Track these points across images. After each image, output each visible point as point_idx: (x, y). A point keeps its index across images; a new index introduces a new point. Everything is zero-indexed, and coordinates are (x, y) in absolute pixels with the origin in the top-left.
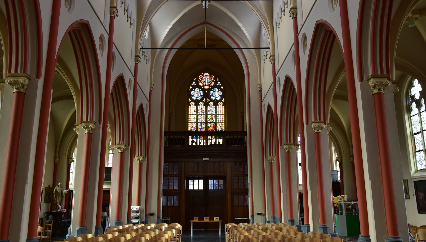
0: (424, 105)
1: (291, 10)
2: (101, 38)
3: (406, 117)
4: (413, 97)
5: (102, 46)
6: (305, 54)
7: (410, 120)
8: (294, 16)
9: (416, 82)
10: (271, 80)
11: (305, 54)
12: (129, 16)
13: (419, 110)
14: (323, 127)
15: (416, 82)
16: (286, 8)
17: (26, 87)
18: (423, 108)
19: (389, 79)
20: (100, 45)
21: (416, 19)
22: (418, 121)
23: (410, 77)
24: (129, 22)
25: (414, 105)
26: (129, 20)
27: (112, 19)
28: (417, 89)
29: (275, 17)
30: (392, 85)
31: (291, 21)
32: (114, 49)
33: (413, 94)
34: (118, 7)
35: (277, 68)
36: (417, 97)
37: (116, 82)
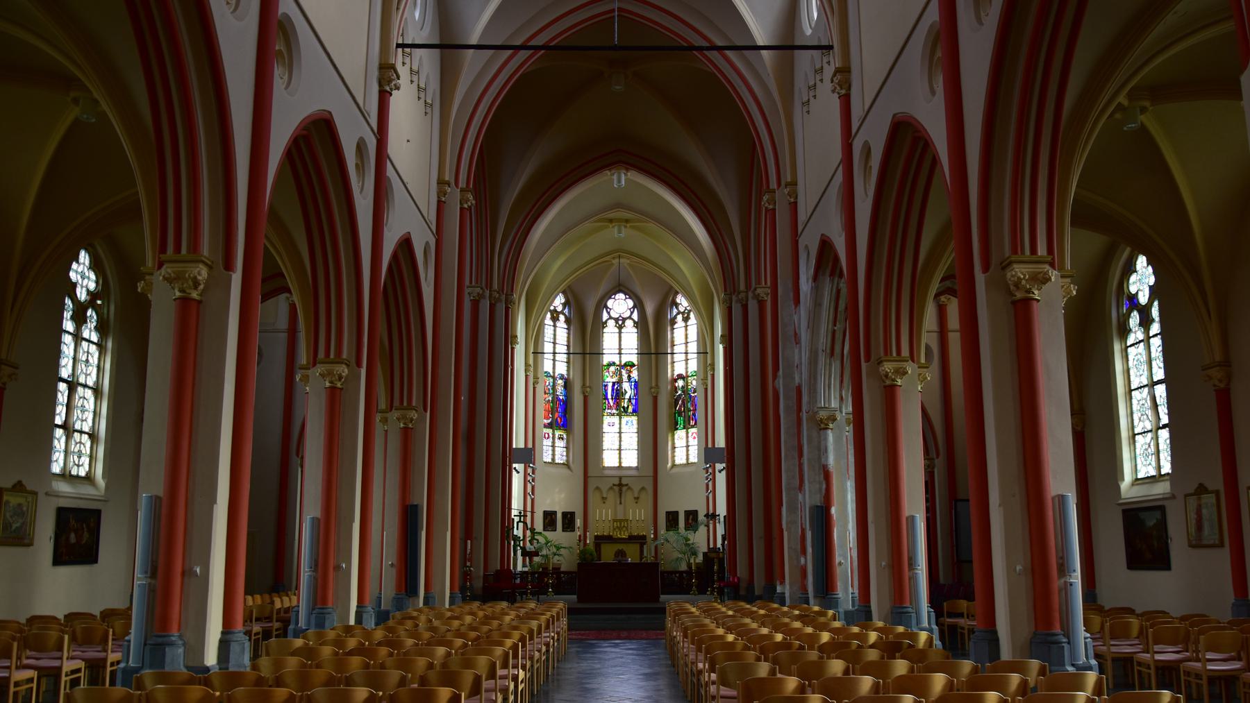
0: (1157, 319)
1: (834, 75)
2: (361, 147)
3: (1117, 347)
4: (1133, 299)
5: (361, 167)
6: (980, 22)
7: (1126, 357)
8: (843, 92)
9: (1142, 261)
10: (837, 154)
11: (980, 22)
12: (415, 68)
13: (1147, 330)
14: (1050, 279)
15: (1142, 261)
16: (825, 66)
17: (202, 287)
18: (1155, 328)
19: (1052, 265)
20: (357, 165)
21: (1143, 110)
22: (1144, 358)
23: (1128, 250)
24: (415, 84)
25: (1134, 319)
26: (422, 95)
27: (384, 97)
28: (1142, 279)
29: (800, 83)
30: (1060, 280)
31: (835, 103)
32: (390, 171)
33: (1133, 289)
34: (399, 67)
35: (856, 112)
36: (1143, 299)
37: (395, 256)
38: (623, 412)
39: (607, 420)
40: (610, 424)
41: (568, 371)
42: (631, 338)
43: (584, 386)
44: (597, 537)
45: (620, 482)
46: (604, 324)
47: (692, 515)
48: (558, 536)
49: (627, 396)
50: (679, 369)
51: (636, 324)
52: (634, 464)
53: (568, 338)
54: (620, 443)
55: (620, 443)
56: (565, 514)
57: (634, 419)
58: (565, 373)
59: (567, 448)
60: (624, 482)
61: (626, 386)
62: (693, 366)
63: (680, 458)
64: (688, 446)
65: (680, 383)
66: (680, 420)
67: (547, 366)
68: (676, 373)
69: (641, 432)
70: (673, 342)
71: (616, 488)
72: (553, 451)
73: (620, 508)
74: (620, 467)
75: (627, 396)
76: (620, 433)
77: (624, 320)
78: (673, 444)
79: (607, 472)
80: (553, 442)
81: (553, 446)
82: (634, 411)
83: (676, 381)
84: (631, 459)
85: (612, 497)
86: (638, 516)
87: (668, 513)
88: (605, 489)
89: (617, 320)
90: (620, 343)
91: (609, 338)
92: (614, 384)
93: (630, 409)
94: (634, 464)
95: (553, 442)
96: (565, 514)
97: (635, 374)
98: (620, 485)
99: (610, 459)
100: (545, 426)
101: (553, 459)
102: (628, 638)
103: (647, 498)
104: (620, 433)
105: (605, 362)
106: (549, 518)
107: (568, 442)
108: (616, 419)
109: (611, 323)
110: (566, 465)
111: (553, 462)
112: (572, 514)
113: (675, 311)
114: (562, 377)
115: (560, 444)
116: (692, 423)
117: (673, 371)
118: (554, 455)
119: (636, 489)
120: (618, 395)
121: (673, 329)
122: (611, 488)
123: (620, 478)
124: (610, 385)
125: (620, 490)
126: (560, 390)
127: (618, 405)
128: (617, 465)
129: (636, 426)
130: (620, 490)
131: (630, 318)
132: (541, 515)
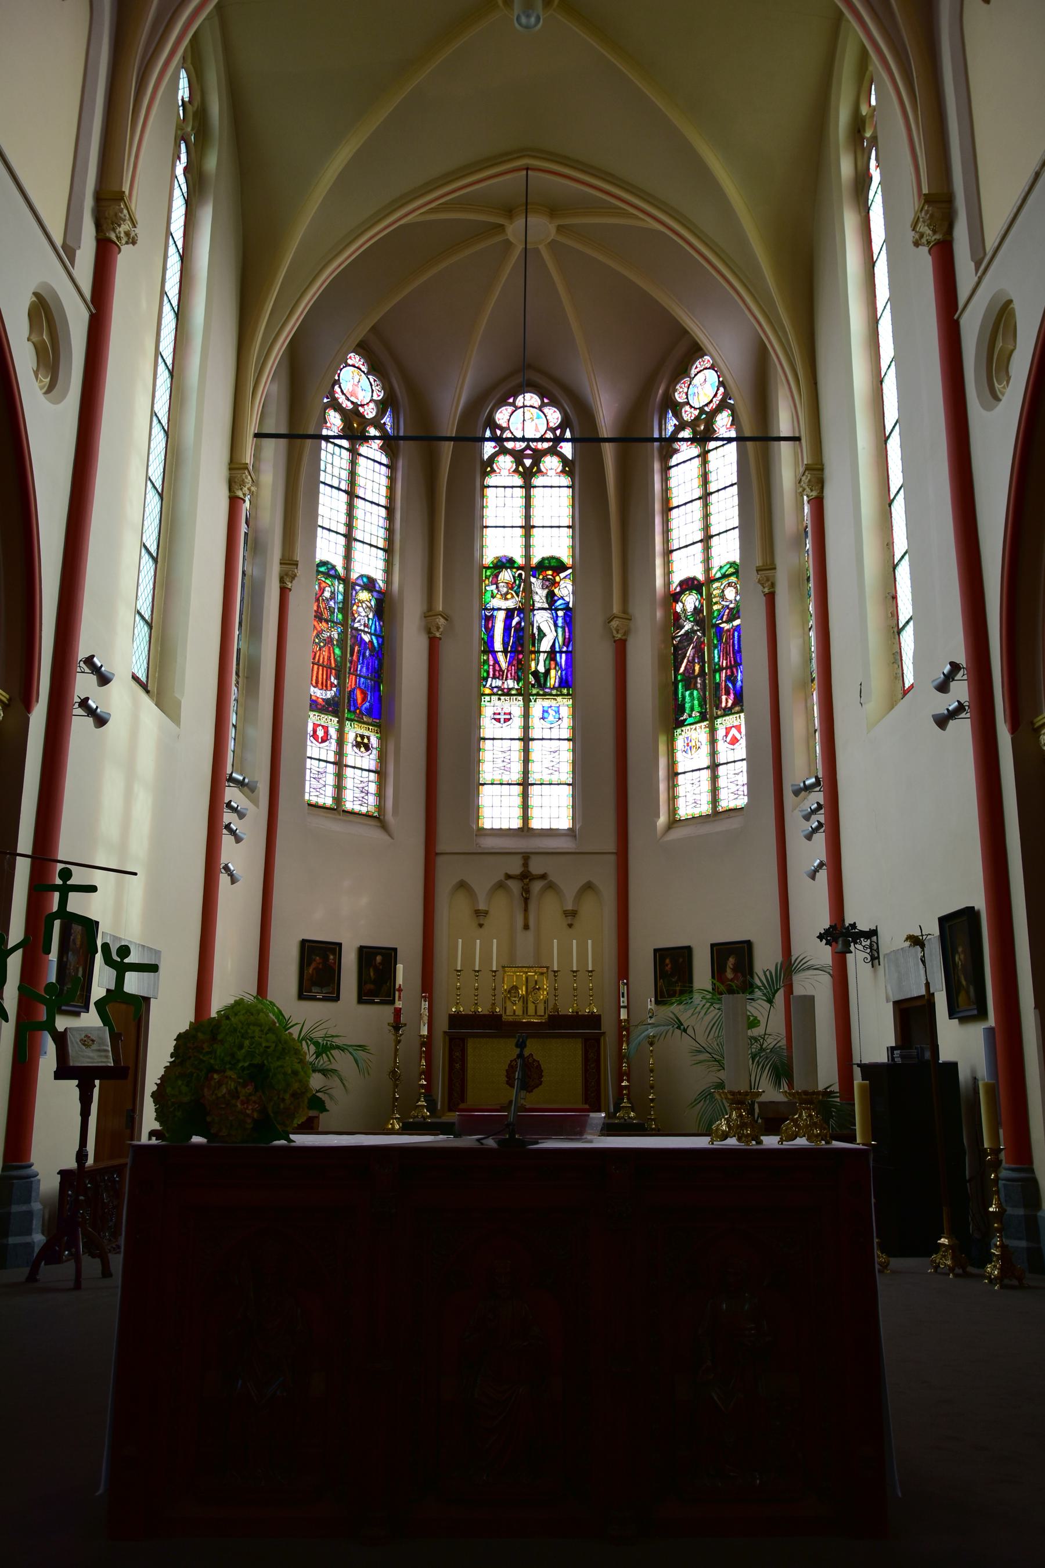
8: (814, 494)
38: (531, 687)
39: (490, 707)
40: (498, 722)
41: (388, 571)
42: (555, 499)
43: (429, 613)
44: (456, 1020)
45: (526, 866)
46: (488, 467)
47: (734, 959)
48: (345, 1016)
49: (545, 645)
50: (687, 565)
51: (568, 467)
52: (564, 822)
53: (391, 489)
54: (527, 770)
55: (527, 770)
56: (366, 954)
57: (564, 706)
58: (379, 575)
59: (380, 773)
60: (536, 867)
61: (542, 619)
62: (727, 550)
63: (692, 799)
64: (714, 767)
65: (690, 601)
66: (691, 700)
67: (328, 549)
68: (677, 578)
69: (581, 739)
70: (666, 500)
71: (515, 886)
72: (339, 776)
73: (525, 941)
74: (525, 830)
75: (545, 645)
76: (526, 740)
77: (538, 456)
78: (672, 763)
79: (489, 843)
80: (340, 752)
81: (340, 764)
82: (565, 682)
83: (676, 597)
84: (554, 810)
85: (502, 911)
86: (566, 959)
87: (661, 954)
88: (482, 886)
89: (518, 456)
90: (526, 517)
91: (500, 501)
92: (510, 614)
93: (553, 679)
94: (564, 822)
95: (340, 752)
96: (366, 954)
97: (565, 590)
98: (526, 877)
99: (497, 810)
100: (315, 705)
101: (338, 799)
102: (574, 772)
103: (600, 914)
104: (526, 740)
105: (488, 559)
106: (318, 965)
107: (382, 757)
108: (515, 706)
109: (505, 463)
110: (378, 819)
111: (337, 809)
112: (390, 955)
113: (672, 423)
114: (370, 584)
115: (362, 762)
116: (727, 701)
117: (668, 573)
118: (339, 787)
119: (570, 889)
120: (522, 640)
121: (666, 469)
122: (500, 886)
123: (526, 857)
124: (501, 616)
125: (526, 890)
126: (363, 615)
127: (519, 668)
128: (516, 824)
129: (567, 722)
130: (526, 890)
131: (553, 451)
132: (293, 954)
